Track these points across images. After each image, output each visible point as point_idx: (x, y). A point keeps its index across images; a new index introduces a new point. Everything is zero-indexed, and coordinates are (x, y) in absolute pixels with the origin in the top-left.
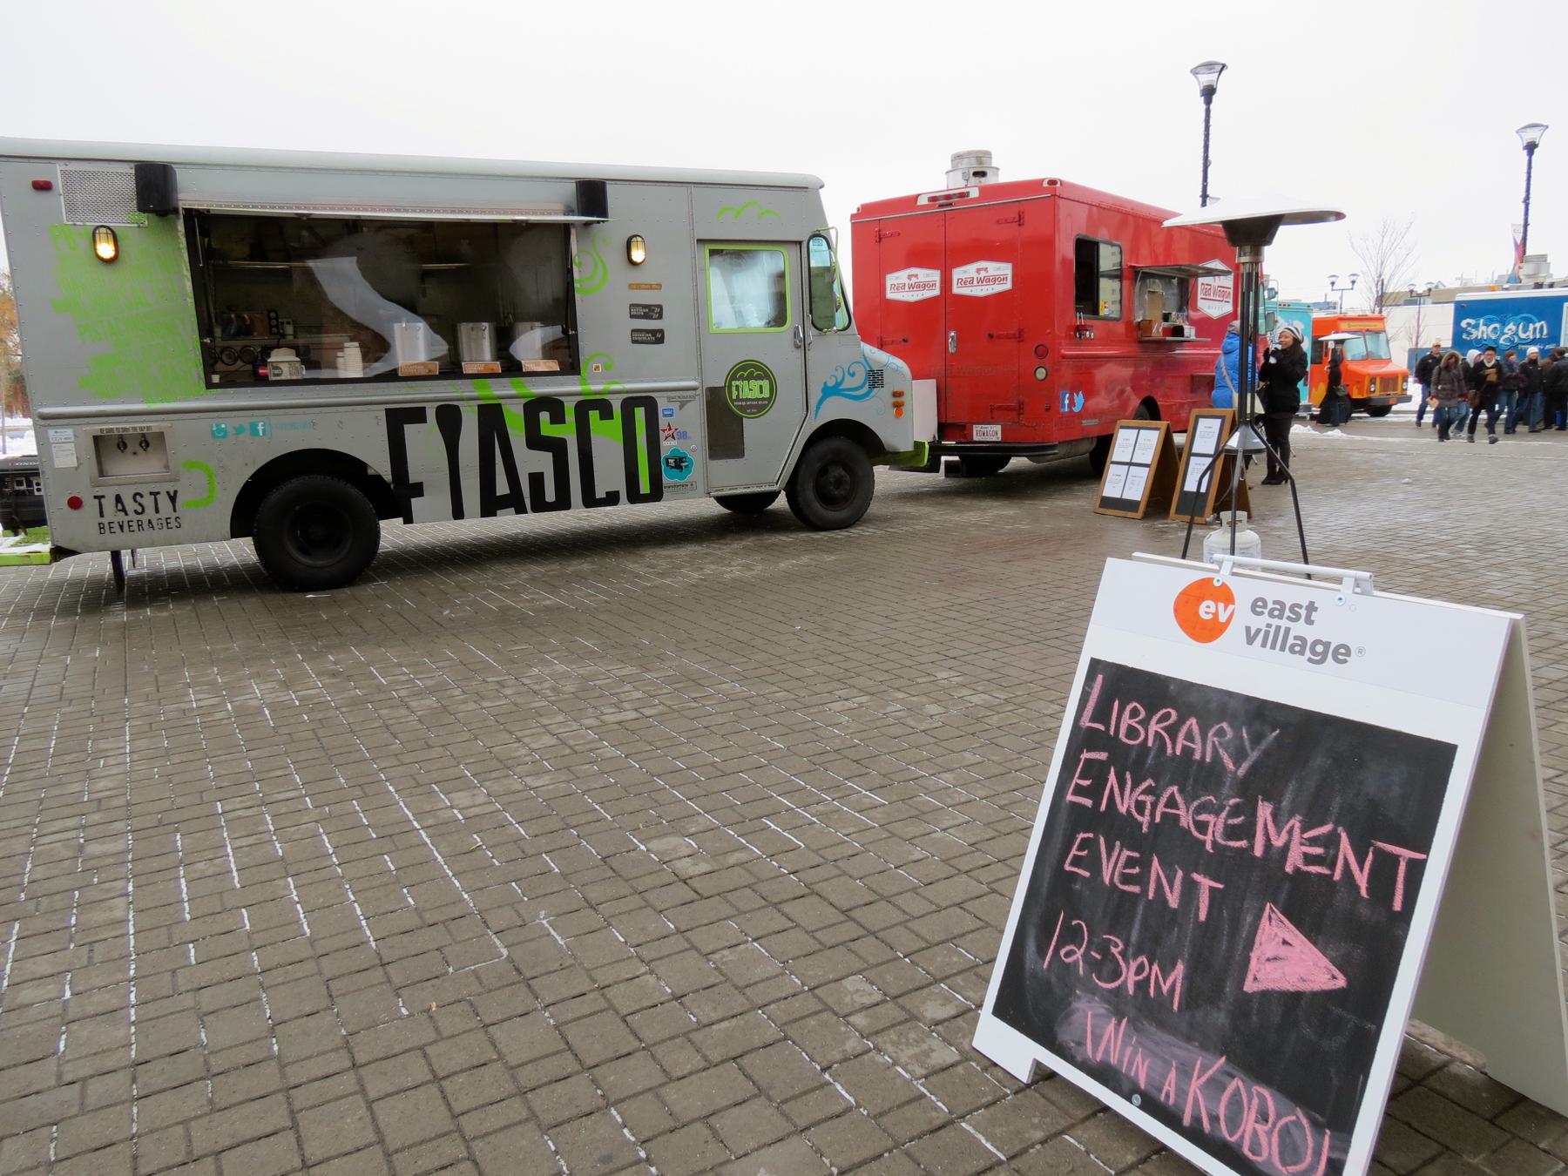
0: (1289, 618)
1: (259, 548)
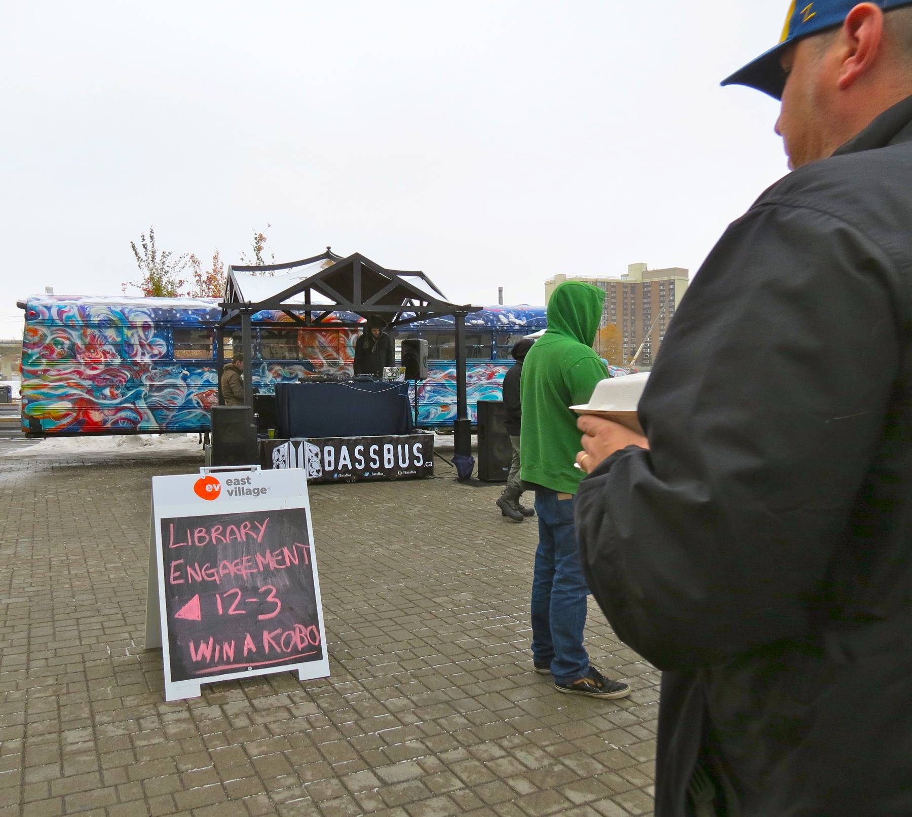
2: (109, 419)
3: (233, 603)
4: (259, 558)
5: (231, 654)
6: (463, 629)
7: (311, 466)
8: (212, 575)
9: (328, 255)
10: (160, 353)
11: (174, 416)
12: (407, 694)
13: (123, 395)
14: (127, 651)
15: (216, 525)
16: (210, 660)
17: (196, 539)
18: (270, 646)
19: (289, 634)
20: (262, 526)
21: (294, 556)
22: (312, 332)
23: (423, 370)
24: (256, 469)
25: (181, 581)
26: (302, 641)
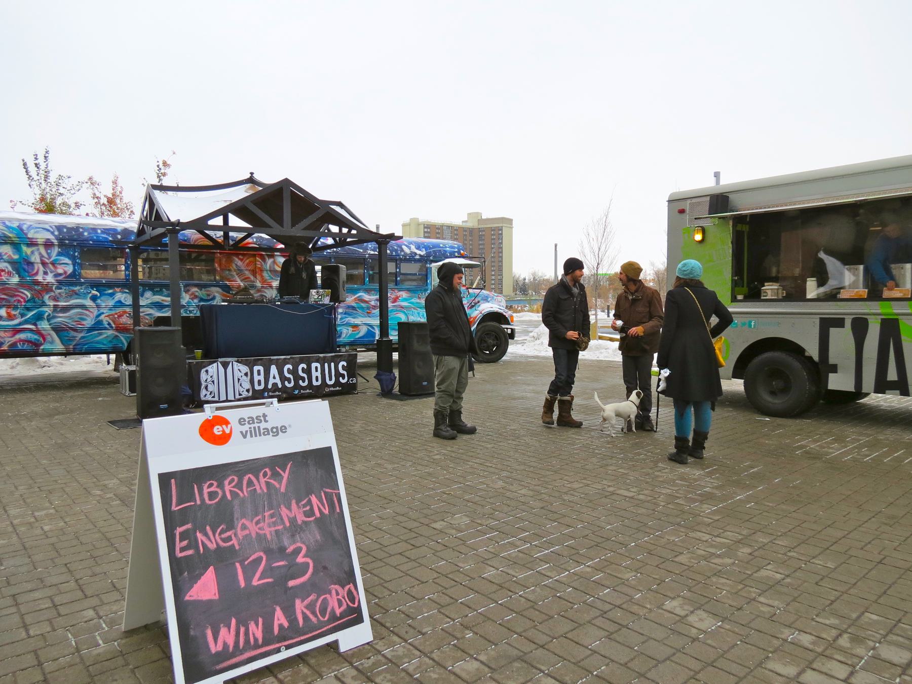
0: (257, 422)
1: (746, 385)
2: (5, 341)
3: (256, 571)
4: (284, 511)
5: (259, 635)
6: (482, 560)
7: (241, 385)
8: (229, 539)
9: (251, 180)
10: (65, 272)
11: (83, 338)
12: (472, 652)
13: (22, 315)
14: (98, 638)
15: (229, 476)
16: (234, 647)
17: (206, 496)
18: (305, 617)
19: (325, 599)
20: (285, 472)
21: (323, 505)
22: (229, 257)
23: (342, 293)
24: (272, 403)
25: (190, 552)
26: (340, 605)
